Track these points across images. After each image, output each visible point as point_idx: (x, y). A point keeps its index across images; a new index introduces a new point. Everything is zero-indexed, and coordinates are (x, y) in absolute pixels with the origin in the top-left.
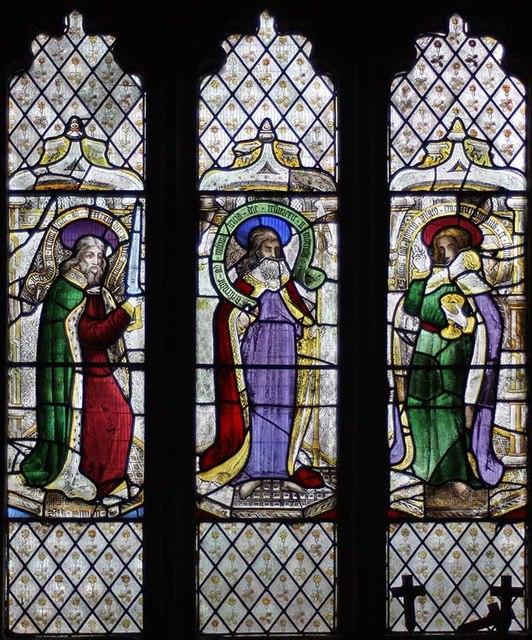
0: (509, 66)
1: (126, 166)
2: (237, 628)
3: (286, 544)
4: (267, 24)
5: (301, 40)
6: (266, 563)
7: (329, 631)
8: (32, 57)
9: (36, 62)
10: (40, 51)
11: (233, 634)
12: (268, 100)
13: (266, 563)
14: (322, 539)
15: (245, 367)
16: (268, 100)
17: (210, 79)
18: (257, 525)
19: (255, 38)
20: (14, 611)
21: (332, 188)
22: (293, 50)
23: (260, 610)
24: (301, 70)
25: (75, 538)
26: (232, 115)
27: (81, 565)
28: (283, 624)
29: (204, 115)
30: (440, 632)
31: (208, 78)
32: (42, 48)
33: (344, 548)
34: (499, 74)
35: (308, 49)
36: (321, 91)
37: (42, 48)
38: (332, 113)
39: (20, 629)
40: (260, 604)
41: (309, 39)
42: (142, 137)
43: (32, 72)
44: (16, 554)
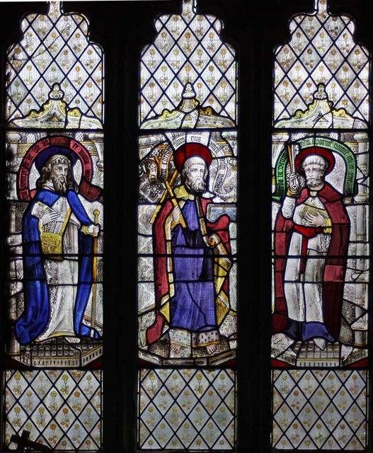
0: (225, 36)
1: (223, 113)
2: (56, 446)
3: (201, 384)
4: (187, 8)
5: (212, 19)
6: (184, 401)
7: (97, 449)
8: (155, 34)
9: (294, 37)
10: (162, 29)
11: (77, 450)
12: (188, 66)
13: (184, 401)
14: (91, 382)
15: (172, 256)
16: (188, 66)
17: (148, 48)
18: (47, 371)
19: (46, 17)
20: (276, 432)
21: (364, 126)
22: (208, 28)
23: (315, 433)
24: (346, 42)
25: (211, 379)
26: (298, 73)
27: (54, 400)
28: (88, 443)
29: (144, 74)
30: (198, 450)
31: (280, 48)
32: (164, 26)
33: (242, 393)
34: (217, 41)
35: (85, 27)
36: (94, 56)
37: (164, 26)
38: (100, 72)
39: (279, 447)
40: (48, 429)
41: (218, 17)
42: (235, 90)
43: (291, 43)
44: (278, 391)
